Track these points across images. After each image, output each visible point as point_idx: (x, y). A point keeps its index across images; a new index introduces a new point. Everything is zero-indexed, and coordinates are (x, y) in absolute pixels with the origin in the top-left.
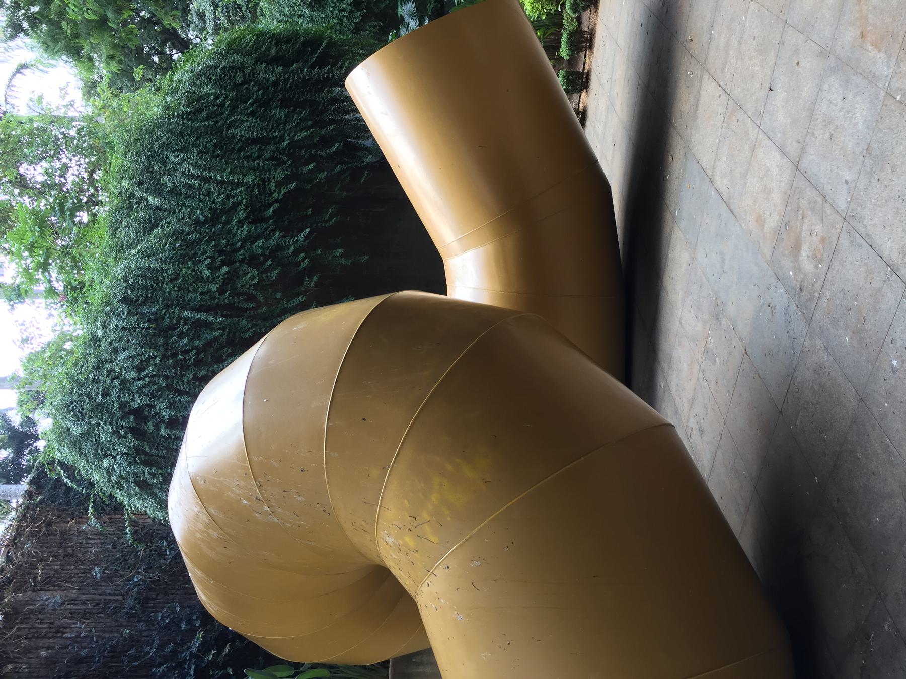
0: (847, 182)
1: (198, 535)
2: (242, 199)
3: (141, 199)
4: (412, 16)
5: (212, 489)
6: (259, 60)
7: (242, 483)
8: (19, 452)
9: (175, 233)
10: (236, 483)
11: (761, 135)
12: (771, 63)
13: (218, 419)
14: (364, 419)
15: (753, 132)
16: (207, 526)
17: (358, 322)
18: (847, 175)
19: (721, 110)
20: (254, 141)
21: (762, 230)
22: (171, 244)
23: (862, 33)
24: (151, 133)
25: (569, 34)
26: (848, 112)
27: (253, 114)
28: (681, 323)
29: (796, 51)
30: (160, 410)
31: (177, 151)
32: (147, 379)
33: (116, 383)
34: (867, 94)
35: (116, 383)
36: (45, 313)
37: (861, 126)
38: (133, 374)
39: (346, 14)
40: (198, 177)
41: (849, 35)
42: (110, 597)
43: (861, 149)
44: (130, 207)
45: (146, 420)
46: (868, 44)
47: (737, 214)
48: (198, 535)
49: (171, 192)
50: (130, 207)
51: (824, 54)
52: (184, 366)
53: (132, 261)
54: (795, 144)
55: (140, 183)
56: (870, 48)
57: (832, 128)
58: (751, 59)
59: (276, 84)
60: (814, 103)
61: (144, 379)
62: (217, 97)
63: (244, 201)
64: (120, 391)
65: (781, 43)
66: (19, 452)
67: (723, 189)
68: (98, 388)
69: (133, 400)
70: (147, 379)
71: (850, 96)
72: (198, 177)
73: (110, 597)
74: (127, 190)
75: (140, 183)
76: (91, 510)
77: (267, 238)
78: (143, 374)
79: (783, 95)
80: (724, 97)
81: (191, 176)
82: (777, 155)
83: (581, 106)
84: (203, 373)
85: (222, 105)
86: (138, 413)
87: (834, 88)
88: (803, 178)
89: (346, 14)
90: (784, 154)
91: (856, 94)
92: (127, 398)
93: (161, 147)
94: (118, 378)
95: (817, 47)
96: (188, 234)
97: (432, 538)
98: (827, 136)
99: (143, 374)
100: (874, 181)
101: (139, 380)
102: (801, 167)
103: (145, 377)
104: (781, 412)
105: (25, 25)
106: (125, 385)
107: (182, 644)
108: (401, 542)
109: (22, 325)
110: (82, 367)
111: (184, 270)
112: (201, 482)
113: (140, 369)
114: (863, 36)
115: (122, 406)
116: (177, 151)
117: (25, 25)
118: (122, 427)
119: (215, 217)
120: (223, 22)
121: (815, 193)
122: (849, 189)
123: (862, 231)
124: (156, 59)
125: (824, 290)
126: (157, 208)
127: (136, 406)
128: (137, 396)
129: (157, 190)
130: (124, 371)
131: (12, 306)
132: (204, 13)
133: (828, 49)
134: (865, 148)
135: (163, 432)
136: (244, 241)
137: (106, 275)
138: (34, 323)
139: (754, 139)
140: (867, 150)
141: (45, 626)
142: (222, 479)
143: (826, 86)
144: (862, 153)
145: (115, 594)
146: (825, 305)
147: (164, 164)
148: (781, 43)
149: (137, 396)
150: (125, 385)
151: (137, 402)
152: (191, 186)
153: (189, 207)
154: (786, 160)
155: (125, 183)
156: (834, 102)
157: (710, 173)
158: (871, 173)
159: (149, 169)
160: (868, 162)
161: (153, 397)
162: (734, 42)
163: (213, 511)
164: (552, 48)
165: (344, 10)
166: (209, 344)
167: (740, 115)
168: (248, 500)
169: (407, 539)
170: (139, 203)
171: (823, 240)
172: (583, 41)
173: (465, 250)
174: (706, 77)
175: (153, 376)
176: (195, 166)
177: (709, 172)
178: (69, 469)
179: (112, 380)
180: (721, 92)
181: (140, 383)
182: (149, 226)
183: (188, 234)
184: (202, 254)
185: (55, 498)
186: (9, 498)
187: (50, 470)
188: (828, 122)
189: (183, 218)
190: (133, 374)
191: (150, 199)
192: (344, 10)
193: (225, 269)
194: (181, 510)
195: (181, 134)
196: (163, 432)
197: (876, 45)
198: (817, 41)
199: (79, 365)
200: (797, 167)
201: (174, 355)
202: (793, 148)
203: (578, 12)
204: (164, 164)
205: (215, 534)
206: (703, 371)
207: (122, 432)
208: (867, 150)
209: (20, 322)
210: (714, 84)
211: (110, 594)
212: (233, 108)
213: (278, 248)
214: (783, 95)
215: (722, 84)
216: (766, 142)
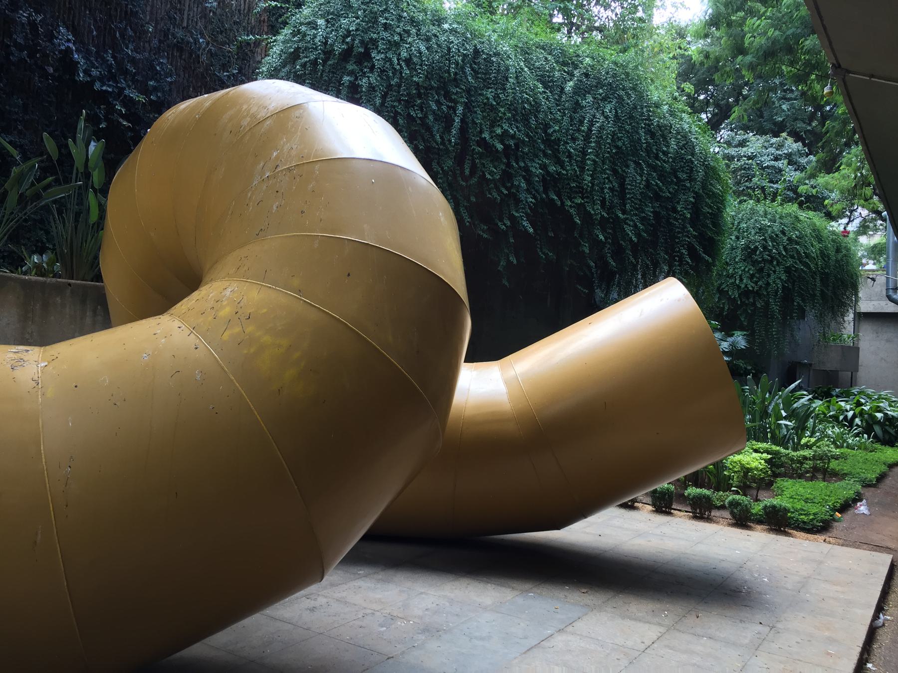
1: (245, 107)
3: (572, 75)
4: (733, 345)
5: (290, 123)
6: (697, 196)
7: (293, 153)
10: (295, 147)
13: (358, 133)
16: (254, 116)
19: (629, 643)
20: (622, 185)
27: (648, 185)
28: (422, 593)
30: (368, 77)
31: (616, 112)
32: (398, 67)
33: (397, 38)
38: (404, 54)
39: (737, 282)
45: (359, 62)
49: (577, 103)
52: (409, 104)
53: (515, 63)
55: (587, 75)
59: (674, 210)
61: (399, 64)
63: (564, 172)
64: (389, 41)
68: (393, 20)
69: (379, 52)
70: (398, 67)
72: (590, 130)
74: (582, 63)
75: (587, 75)
77: (528, 191)
78: (403, 64)
80: (643, 647)
81: (592, 123)
85: (657, 157)
86: (366, 56)
89: (737, 282)
92: (381, 46)
93: (620, 98)
94: (401, 40)
96: (536, 117)
99: (403, 64)
101: (398, 60)
103: (400, 65)
106: (395, 46)
107: (134, 81)
111: (502, 110)
112: (297, 113)
113: (408, 61)
115: (374, 42)
116: (616, 112)
118: (353, 40)
119: (551, 143)
120: (736, 164)
127: (373, 55)
129: (580, 90)
130: (408, 46)
132: (745, 146)
135: (346, 79)
136: (526, 169)
142: (299, 134)
145: (188, 19)
147: (604, 99)
150: (395, 46)
151: (377, 56)
152: (581, 122)
159: (599, 84)
161: (381, 71)
162: (696, 660)
163: (268, 122)
165: (741, 280)
166: (429, 129)
167: (624, 662)
168: (277, 157)
172: (702, 511)
173: (506, 382)
174: (662, 630)
175: (401, 73)
176: (602, 128)
177: (570, 629)
179: (400, 34)
181: (396, 61)
182: (546, 80)
183: (536, 117)
184: (517, 127)
190: (404, 54)
191: (571, 83)
192: (741, 280)
193: (500, 147)
194: (271, 92)
195: (631, 117)
196: (346, 79)
201: (419, 96)
204: (604, 99)
205: (245, 123)
207: (349, 39)
210: (655, 637)
212: (654, 168)
213: (518, 201)
215: (655, 645)
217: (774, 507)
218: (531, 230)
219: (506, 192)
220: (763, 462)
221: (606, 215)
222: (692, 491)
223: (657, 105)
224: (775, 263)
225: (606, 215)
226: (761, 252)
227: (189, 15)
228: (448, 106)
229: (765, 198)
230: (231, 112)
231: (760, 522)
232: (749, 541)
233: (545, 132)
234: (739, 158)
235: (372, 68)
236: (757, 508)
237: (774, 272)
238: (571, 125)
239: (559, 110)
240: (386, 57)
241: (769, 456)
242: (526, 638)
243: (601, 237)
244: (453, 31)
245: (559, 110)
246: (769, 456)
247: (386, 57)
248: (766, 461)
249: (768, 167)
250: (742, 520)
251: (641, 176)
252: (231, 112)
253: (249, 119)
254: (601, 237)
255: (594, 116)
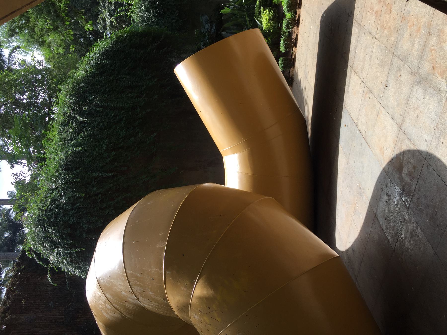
0: (426, 141)
1: (101, 306)
2: (123, 117)
4: (207, 22)
5: (107, 285)
7: (122, 284)
8: (14, 233)
9: (90, 136)
10: (119, 283)
11: (382, 108)
12: (386, 73)
13: (109, 253)
14: (183, 255)
15: (378, 105)
16: (105, 303)
17: (180, 202)
18: (427, 137)
19: (361, 91)
21: (383, 156)
22: (87, 140)
23: (433, 67)
24: (79, 84)
25: (284, 40)
26: (426, 105)
28: (342, 194)
29: (399, 69)
30: (83, 225)
31: (91, 93)
32: (77, 210)
34: (436, 98)
35: (61, 211)
36: (27, 168)
37: (433, 114)
38: (70, 207)
39: (175, 21)
40: (101, 107)
41: (427, 67)
42: (59, 317)
43: (433, 126)
44: (69, 122)
46: (437, 73)
47: (370, 145)
48: (101, 306)
50: (69, 122)
51: (413, 73)
54: (399, 116)
55: (73, 110)
56: (438, 75)
57: (418, 112)
58: (376, 68)
60: (409, 97)
61: (75, 209)
62: (111, 66)
63: (124, 118)
64: (63, 215)
65: (392, 64)
66: (14, 233)
67: (363, 131)
68: (52, 214)
69: (69, 220)
70: (77, 210)
71: (427, 97)
72: (101, 107)
73: (59, 317)
74: (67, 113)
76: (49, 275)
78: (75, 207)
79: (393, 90)
80: (362, 85)
81: (98, 106)
82: (390, 120)
83: (291, 74)
84: (104, 206)
87: (419, 91)
88: (403, 134)
89: (175, 21)
90: (394, 120)
91: (430, 97)
92: (66, 219)
93: (84, 92)
94: (62, 209)
95: (410, 69)
96: (97, 135)
97: (217, 319)
98: (416, 115)
99: (75, 207)
100: (440, 143)
101: (72, 210)
102: (404, 127)
103: (76, 208)
104: (394, 250)
105: (17, 30)
108: (202, 319)
109: (16, 175)
110: (44, 203)
111: (95, 153)
112: (102, 281)
114: (433, 68)
116: (91, 93)
117: (17, 30)
118: (64, 234)
121: (409, 143)
122: (427, 144)
123: (435, 167)
124: (82, 40)
125: (415, 193)
126: (82, 122)
127: (71, 223)
128: (71, 218)
129: (82, 113)
130: (65, 205)
131: (12, 165)
132: (105, 18)
133: (416, 71)
134: (435, 125)
135: (84, 236)
137: (56, 152)
138: (22, 174)
139: (378, 109)
140: (436, 126)
141: (26, 331)
142: (112, 280)
143: (415, 90)
144: (433, 127)
145: (60, 315)
146: (416, 201)
147: (85, 100)
148: (392, 64)
149: (71, 218)
151: (72, 221)
152: (98, 111)
153: (97, 121)
154: (395, 123)
155: (66, 109)
156: (419, 99)
157: (356, 122)
158: (438, 139)
159: (77, 102)
160: (437, 134)
161: (79, 218)
162: (367, 58)
163: (108, 296)
164: (274, 46)
165: (174, 19)
167: (371, 95)
168: (125, 292)
169: (205, 318)
170: (73, 120)
171: (414, 167)
172: (292, 43)
173: (234, 153)
174: (353, 73)
175: (79, 208)
176: (100, 101)
177: (355, 120)
178: (39, 255)
179: (59, 210)
180: (361, 82)
181: (74, 211)
183: (97, 135)
184: (103, 144)
185: (30, 269)
186: (9, 259)
187: (29, 254)
188: (416, 109)
189: (94, 127)
190: (70, 207)
191: (78, 118)
192: (174, 19)
193: (114, 153)
194: (92, 291)
196: (84, 236)
197: (440, 74)
198: (410, 67)
199: (43, 202)
200: (400, 127)
202: (398, 118)
203: (289, 29)
204: (85, 100)
205: (109, 306)
206: (354, 220)
207: (64, 236)
208: (436, 126)
209: (15, 173)
210: (357, 77)
211: (58, 315)
214: (393, 90)
215: (361, 78)
216: (384, 112)
217: (287, 7)
218: (155, 134)
219: (136, 149)
220: (265, 12)
221: (144, 95)
222: (282, 49)
223: (87, 71)
224: (164, 2)
225: (144, 95)
226: (159, 10)
227: (58, 315)
228: (95, 182)
229: (131, 9)
230: (104, 314)
231: (295, 13)
232: (305, 21)
233: (104, 129)
234: (112, 22)
235: (78, 223)
236: (288, 15)
237: (168, 2)
238: (100, 116)
239: (93, 123)
240: (72, 216)
241: (262, 7)
242: (361, 144)
243: (156, 97)
244: (55, 182)
245: (93, 123)
246: (262, 7)
247: (72, 216)
248: (264, 10)
249: (115, 7)
250: (295, 22)
251: (124, 78)
252: (104, 314)
253: (107, 305)
254: (156, 97)
255: (94, 105)
